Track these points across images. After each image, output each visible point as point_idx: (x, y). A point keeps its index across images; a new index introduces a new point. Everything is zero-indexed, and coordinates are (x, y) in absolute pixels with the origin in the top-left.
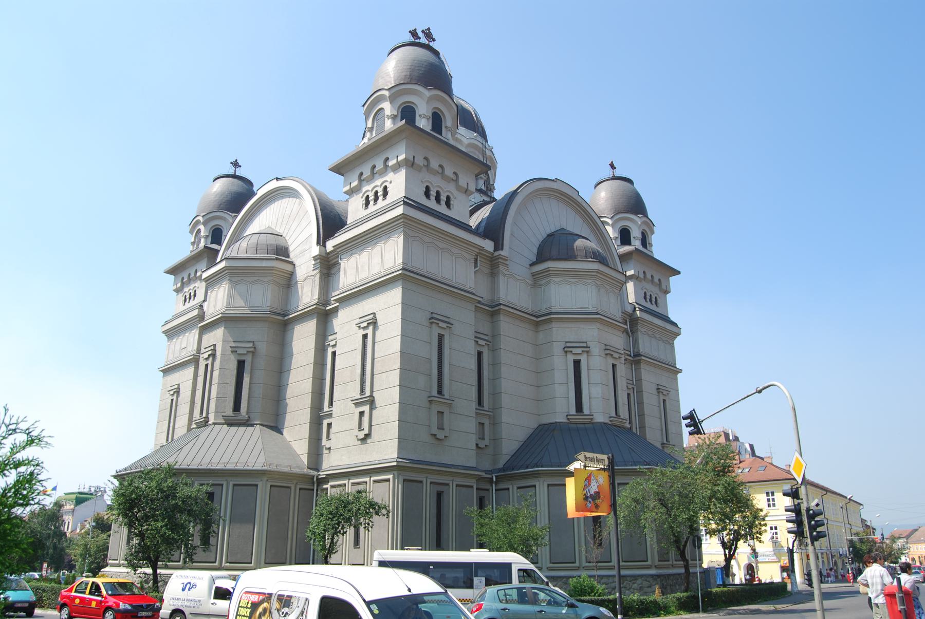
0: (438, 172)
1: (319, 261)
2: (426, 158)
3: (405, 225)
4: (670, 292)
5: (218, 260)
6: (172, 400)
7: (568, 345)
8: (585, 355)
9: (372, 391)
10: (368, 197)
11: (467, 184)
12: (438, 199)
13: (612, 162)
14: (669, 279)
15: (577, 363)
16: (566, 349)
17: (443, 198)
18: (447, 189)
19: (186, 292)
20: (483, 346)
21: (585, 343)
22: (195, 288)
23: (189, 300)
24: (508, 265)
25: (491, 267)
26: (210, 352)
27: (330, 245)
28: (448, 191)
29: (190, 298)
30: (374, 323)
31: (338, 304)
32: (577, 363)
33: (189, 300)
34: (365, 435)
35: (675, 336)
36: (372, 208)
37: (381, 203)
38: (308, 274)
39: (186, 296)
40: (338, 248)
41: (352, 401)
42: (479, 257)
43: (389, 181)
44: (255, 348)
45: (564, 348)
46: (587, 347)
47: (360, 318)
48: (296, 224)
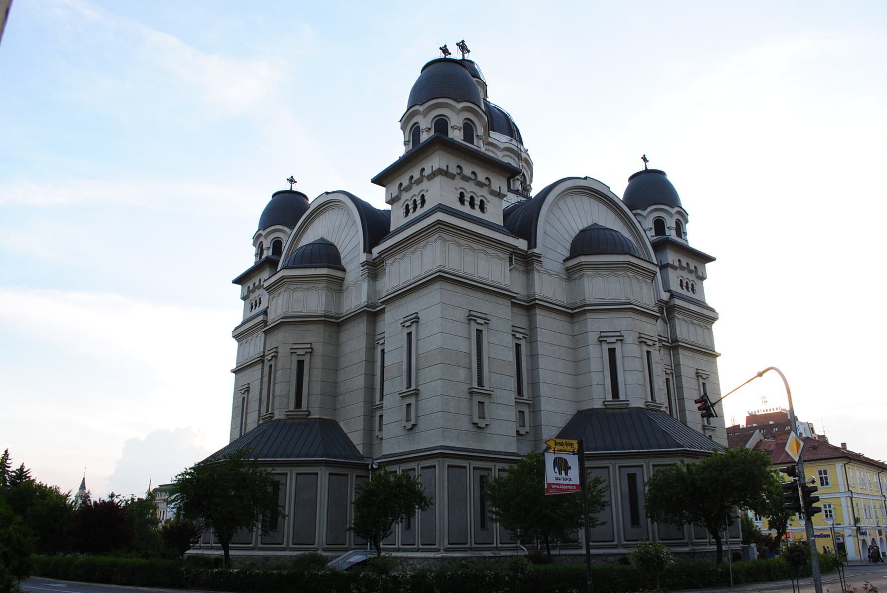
2: (459, 167)
5: (279, 269)
6: (244, 398)
7: (603, 334)
10: (407, 206)
11: (500, 187)
12: (687, 288)
13: (644, 155)
15: (612, 352)
17: (477, 202)
18: (481, 193)
20: (520, 339)
24: (541, 262)
26: (273, 354)
27: (376, 251)
28: (692, 280)
29: (256, 305)
32: (612, 352)
36: (412, 216)
37: (420, 211)
39: (252, 303)
41: (400, 394)
43: (426, 190)
45: (599, 338)
47: (404, 318)
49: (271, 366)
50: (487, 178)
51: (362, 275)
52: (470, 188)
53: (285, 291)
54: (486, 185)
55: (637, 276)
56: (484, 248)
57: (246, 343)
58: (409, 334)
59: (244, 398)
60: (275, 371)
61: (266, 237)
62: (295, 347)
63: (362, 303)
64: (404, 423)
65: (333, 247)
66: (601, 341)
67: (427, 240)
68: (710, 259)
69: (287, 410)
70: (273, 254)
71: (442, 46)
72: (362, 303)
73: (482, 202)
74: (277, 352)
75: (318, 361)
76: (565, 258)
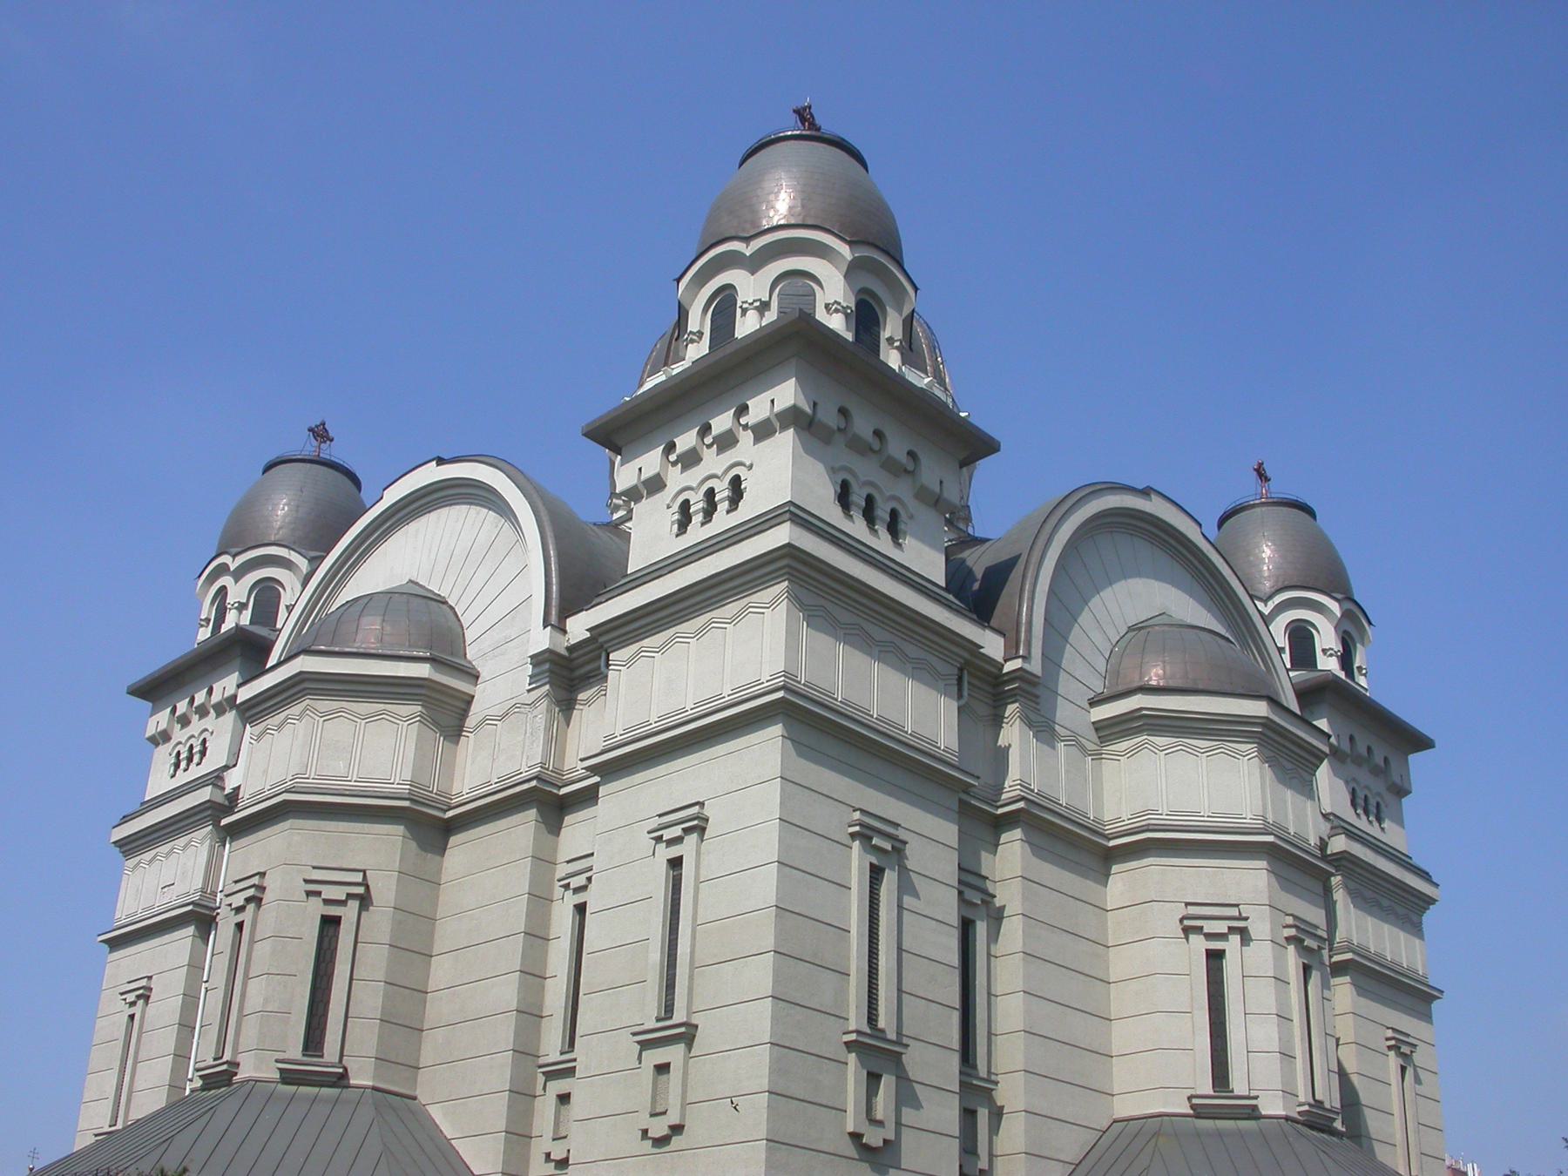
0: (871, 449)
1: (547, 666)
2: (843, 412)
3: (794, 576)
4: (1411, 792)
5: (272, 662)
6: (132, 1017)
7: (1192, 910)
8: (1235, 939)
9: (235, 1051)
10: (686, 505)
11: (941, 482)
13: (1260, 465)
14: (1407, 759)
15: (1215, 958)
16: (1186, 922)
17: (883, 512)
19: (180, 743)
20: (976, 905)
21: (1237, 909)
22: (205, 735)
23: (188, 765)
24: (1037, 697)
25: (994, 701)
26: (251, 892)
27: (579, 626)
28: (894, 498)
29: (190, 759)
30: (699, 827)
31: (596, 779)
33: (188, 765)
34: (671, 1127)
35: (1425, 906)
38: (513, 702)
39: (179, 753)
40: (601, 635)
41: (634, 1034)
42: (966, 672)
43: (210, 730)
44: (367, 887)
45: (1181, 921)
46: (1241, 918)
47: (660, 816)
48: (482, 574)
49: (240, 926)
50: (911, 454)
51: (529, 691)
52: (866, 472)
53: (300, 717)
54: (906, 471)
55: (1281, 759)
56: (898, 641)
57: (151, 861)
58: (676, 863)
59: (132, 1017)
60: (252, 942)
61: (238, 575)
62: (319, 878)
63: (192, 891)
64: (645, 1121)
65: (444, 607)
66: (1187, 931)
67: (139, 858)
68: (1421, 743)
69: (281, 1056)
70: (252, 622)
71: (314, 423)
72: (464, 793)
73: (894, 514)
74: (262, 889)
75: (379, 922)
76: (1092, 695)
